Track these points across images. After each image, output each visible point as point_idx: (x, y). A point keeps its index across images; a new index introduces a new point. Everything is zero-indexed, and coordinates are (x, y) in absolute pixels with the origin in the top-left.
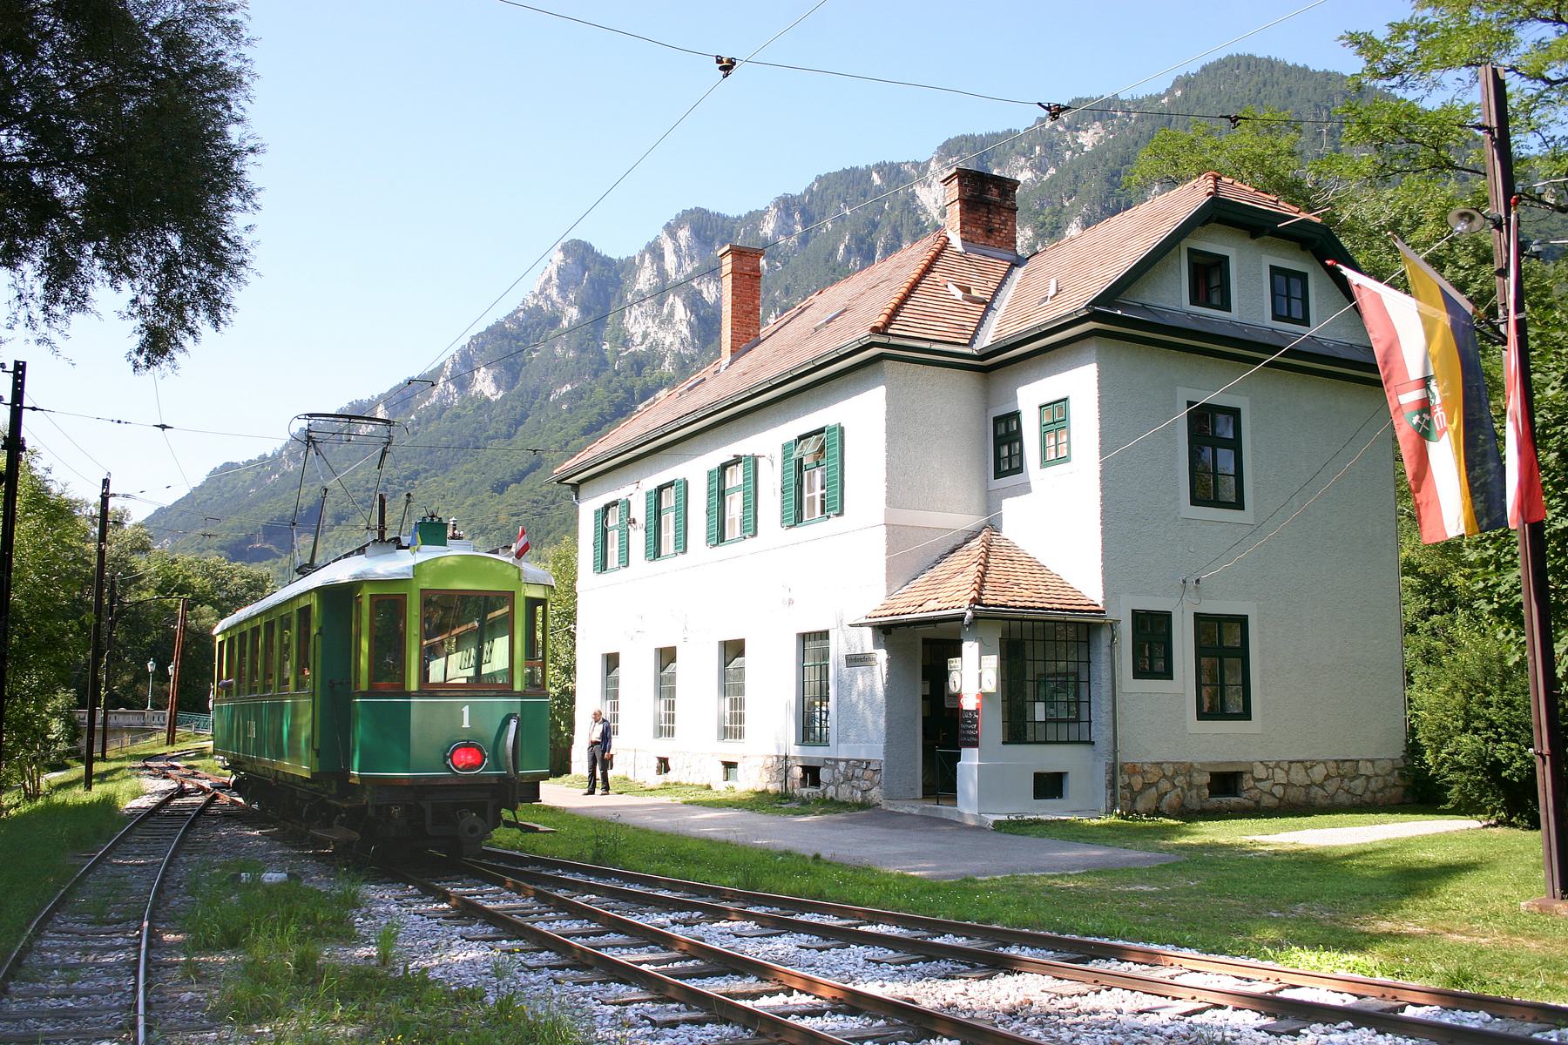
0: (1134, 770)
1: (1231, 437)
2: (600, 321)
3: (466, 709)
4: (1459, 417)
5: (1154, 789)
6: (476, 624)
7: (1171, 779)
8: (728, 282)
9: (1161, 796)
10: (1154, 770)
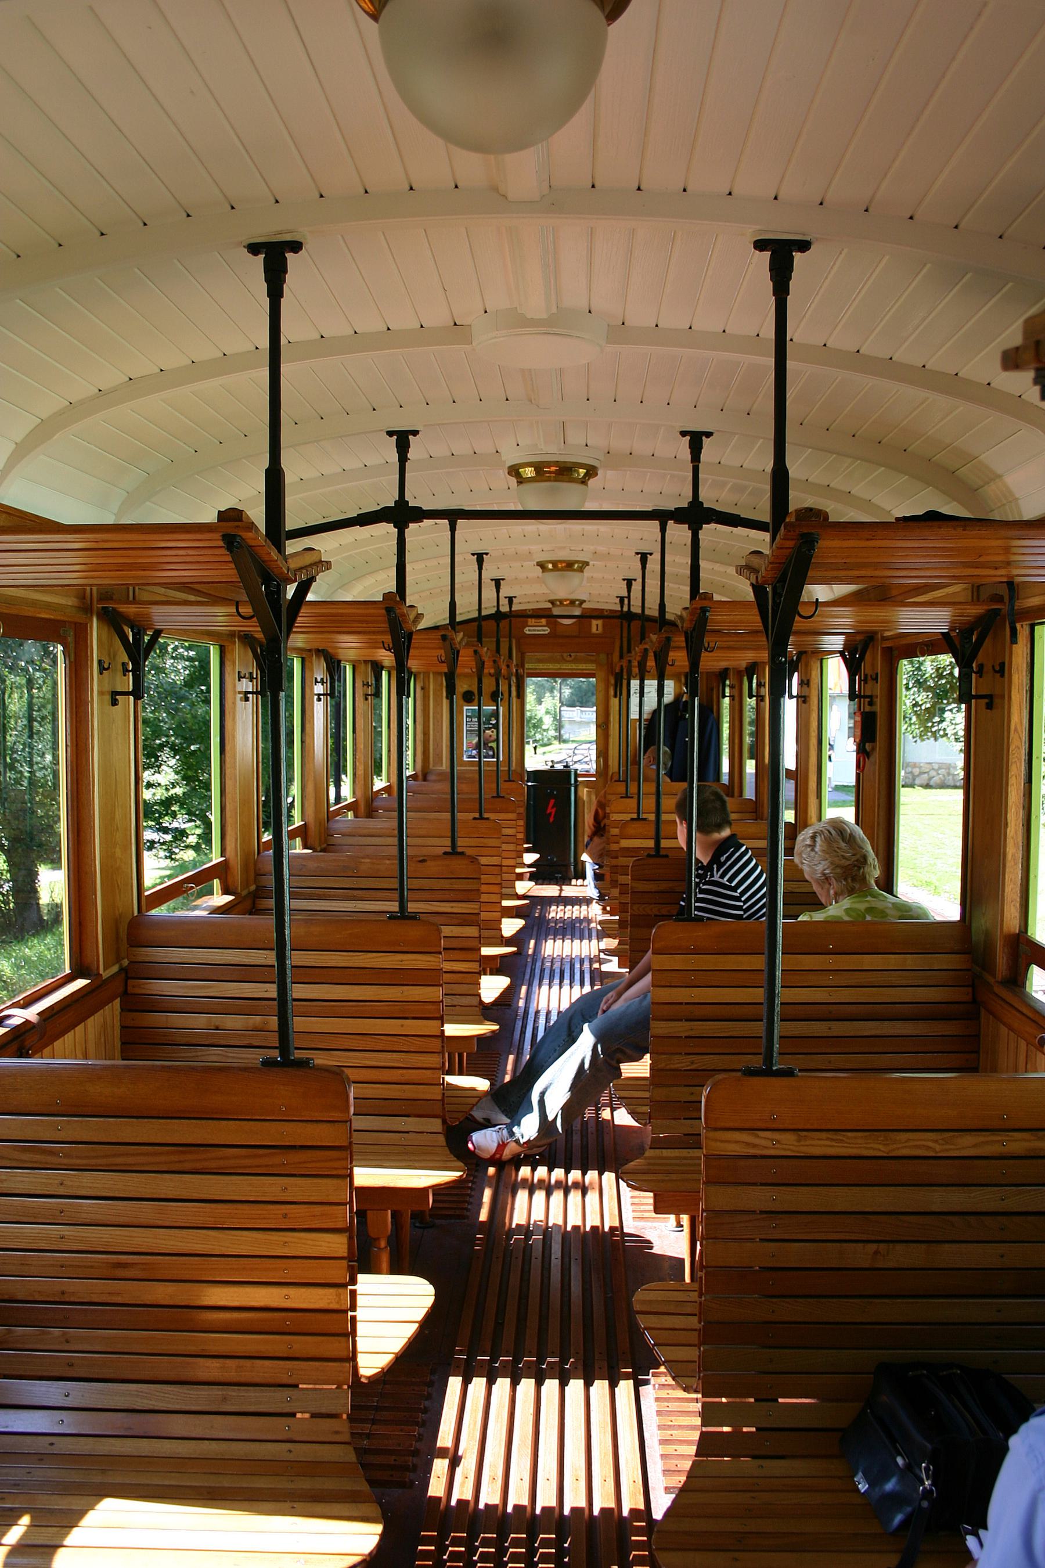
0: (915, 765)
1: (457, 620)
2: (53, 754)
3: (696, 904)
4: (48, 606)
5: (926, 775)
6: (585, 789)
7: (937, 770)
8: (287, 907)
9: (930, 778)
10: (928, 766)
